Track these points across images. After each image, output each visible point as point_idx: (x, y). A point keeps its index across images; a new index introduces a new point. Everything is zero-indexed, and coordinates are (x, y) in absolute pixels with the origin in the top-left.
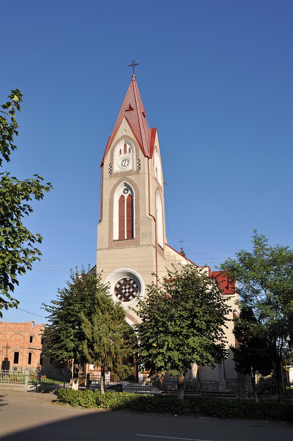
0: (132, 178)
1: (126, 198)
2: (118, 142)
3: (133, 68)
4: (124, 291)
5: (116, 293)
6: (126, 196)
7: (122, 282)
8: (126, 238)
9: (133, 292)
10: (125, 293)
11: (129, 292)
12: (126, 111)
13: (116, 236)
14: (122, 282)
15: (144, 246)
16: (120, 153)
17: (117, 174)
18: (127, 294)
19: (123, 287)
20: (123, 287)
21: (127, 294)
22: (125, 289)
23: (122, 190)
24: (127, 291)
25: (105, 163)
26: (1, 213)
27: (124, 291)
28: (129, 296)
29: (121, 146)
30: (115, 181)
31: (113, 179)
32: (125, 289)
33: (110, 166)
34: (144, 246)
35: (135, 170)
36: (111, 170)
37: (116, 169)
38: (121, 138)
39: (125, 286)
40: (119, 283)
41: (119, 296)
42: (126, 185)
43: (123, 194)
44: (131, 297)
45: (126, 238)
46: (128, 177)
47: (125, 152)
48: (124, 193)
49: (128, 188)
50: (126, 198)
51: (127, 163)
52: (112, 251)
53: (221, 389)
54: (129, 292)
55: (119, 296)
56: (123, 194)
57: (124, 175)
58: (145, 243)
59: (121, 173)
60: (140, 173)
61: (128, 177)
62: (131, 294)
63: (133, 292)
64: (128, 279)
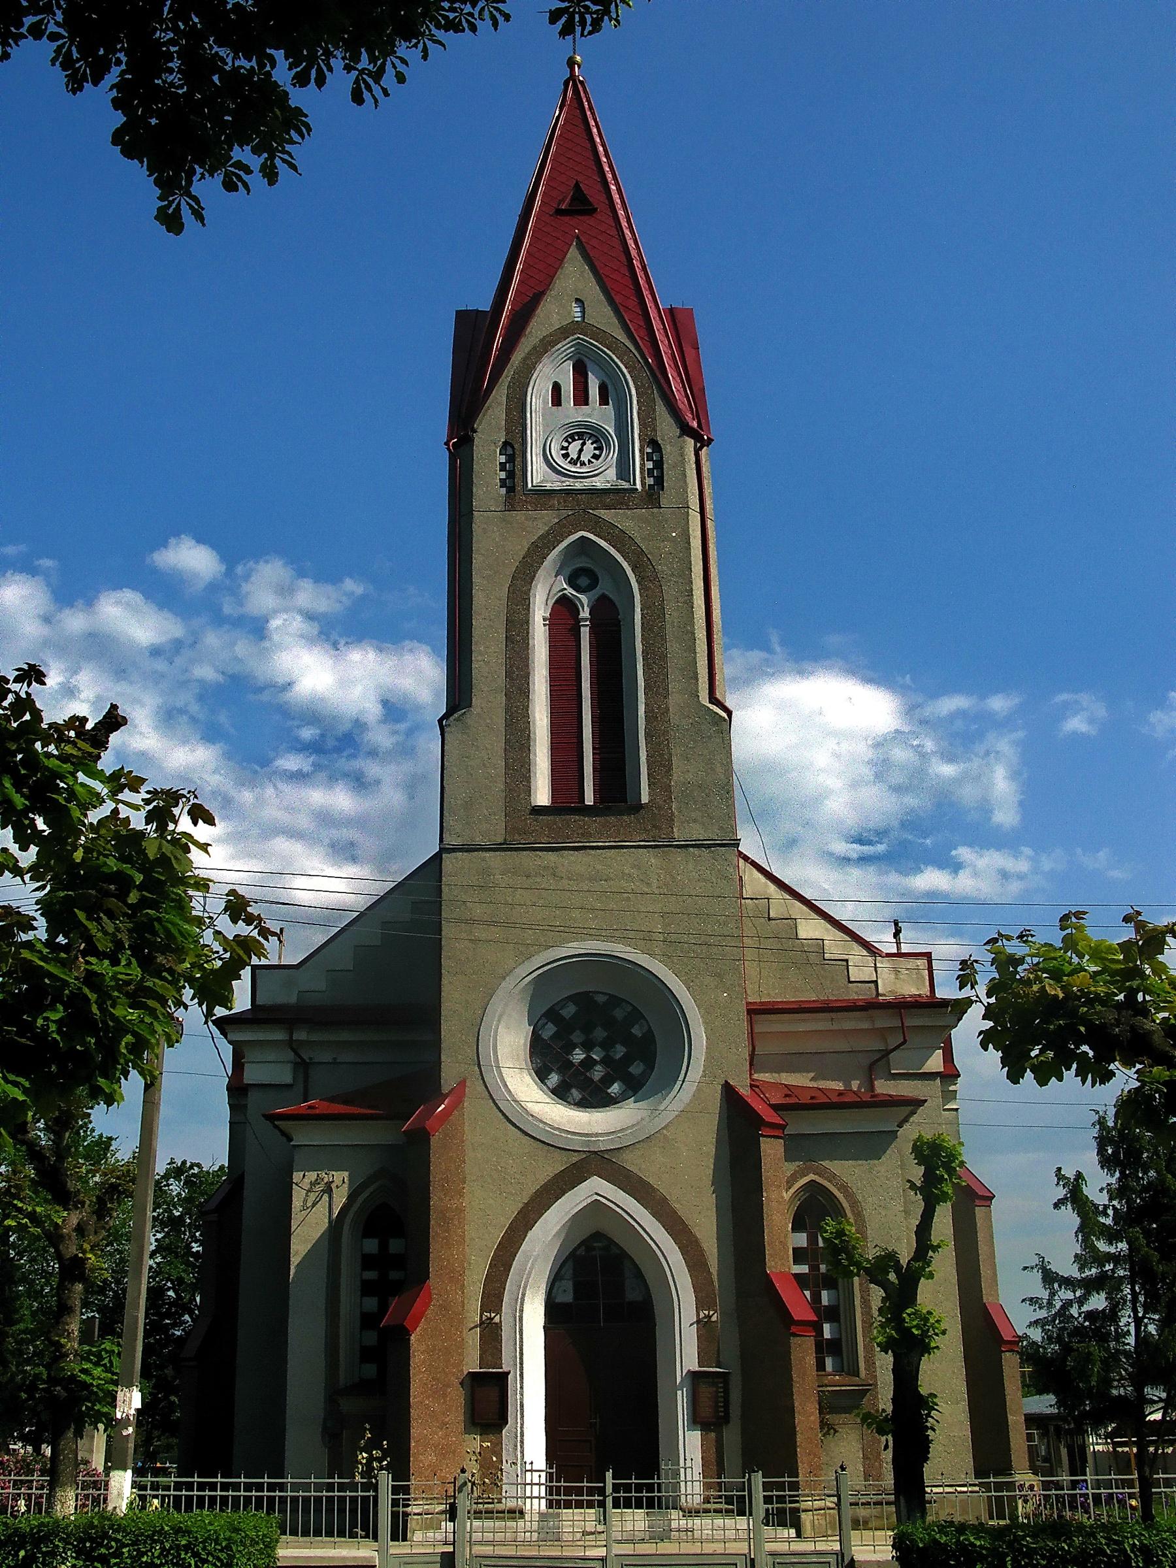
2: (545, 346)
4: (578, 1056)
8: (589, 800)
9: (628, 1060)
10: (588, 1063)
13: (542, 795)
14: (569, 1011)
16: (557, 400)
20: (577, 1037)
21: (598, 1073)
26: (1174, 1176)
27: (578, 1056)
29: (554, 371)
32: (588, 1046)
35: (639, 486)
38: (565, 332)
39: (587, 1029)
45: (589, 800)
46: (603, 514)
47: (582, 398)
49: (585, 569)
50: (585, 613)
53: (171, 827)
57: (581, 503)
58: (697, 832)
60: (664, 502)
61: (603, 514)
63: (628, 1060)
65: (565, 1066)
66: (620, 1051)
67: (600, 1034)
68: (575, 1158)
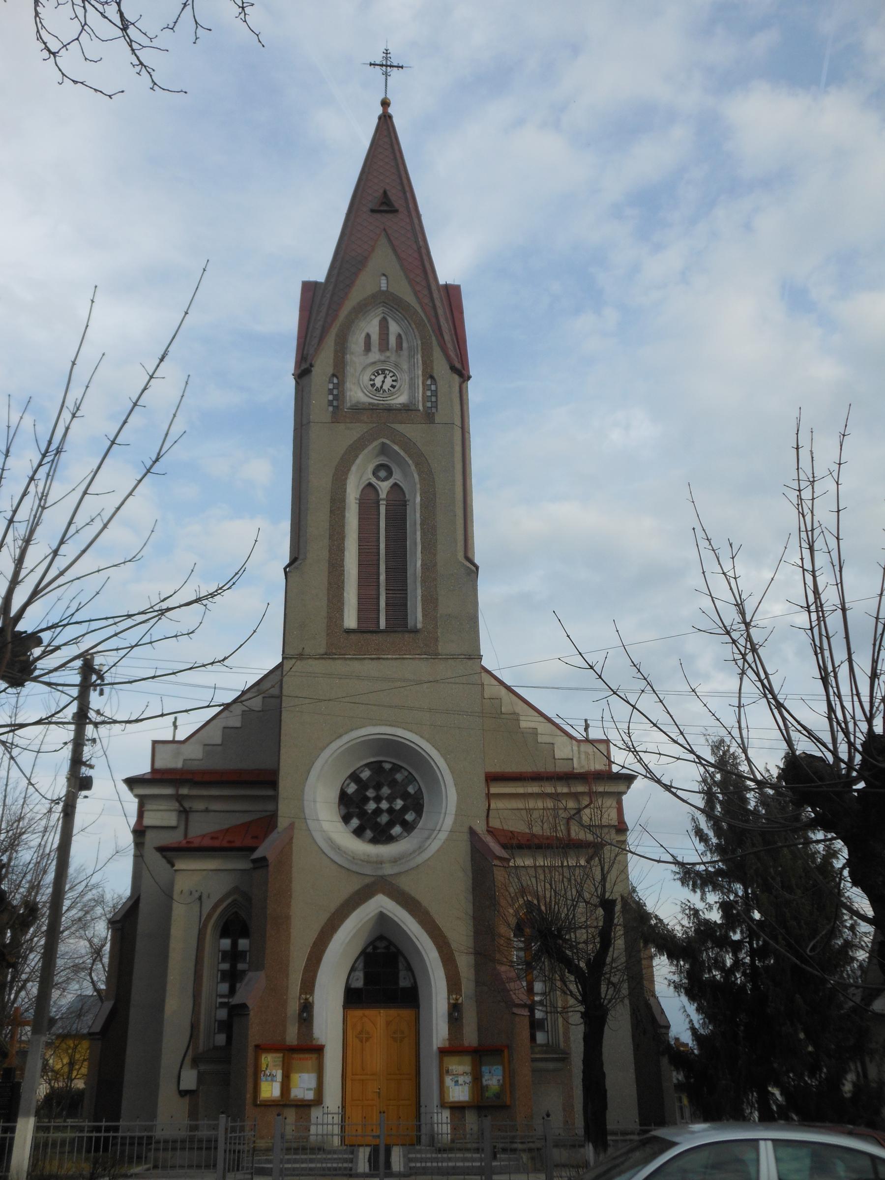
0: (411, 431)
1: (383, 495)
3: (386, 74)
4: (371, 806)
5: (344, 811)
6: (384, 487)
7: (366, 774)
8: (383, 624)
10: (378, 812)
11: (390, 811)
12: (373, 211)
13: (351, 620)
14: (366, 774)
15: (454, 657)
17: (358, 410)
18: (384, 819)
19: (371, 793)
20: (371, 793)
21: (384, 819)
22: (378, 799)
23: (371, 467)
24: (384, 805)
25: (316, 370)
27: (371, 806)
28: (391, 824)
30: (349, 434)
31: (342, 426)
32: (378, 799)
33: (330, 382)
34: (454, 657)
36: (336, 398)
37: (357, 393)
39: (378, 787)
40: (354, 777)
41: (355, 822)
42: (384, 450)
43: (374, 481)
44: (397, 830)
45: (383, 624)
46: (393, 426)
48: (378, 478)
50: (383, 495)
51: (389, 381)
52: (339, 666)
54: (390, 811)
55: (355, 822)
56: (374, 481)
59: (372, 409)
60: (437, 419)
61: (393, 426)
62: (396, 817)
63: (404, 810)
64: (387, 766)
65: (362, 815)
66: (399, 804)
67: (386, 791)
68: (368, 880)
